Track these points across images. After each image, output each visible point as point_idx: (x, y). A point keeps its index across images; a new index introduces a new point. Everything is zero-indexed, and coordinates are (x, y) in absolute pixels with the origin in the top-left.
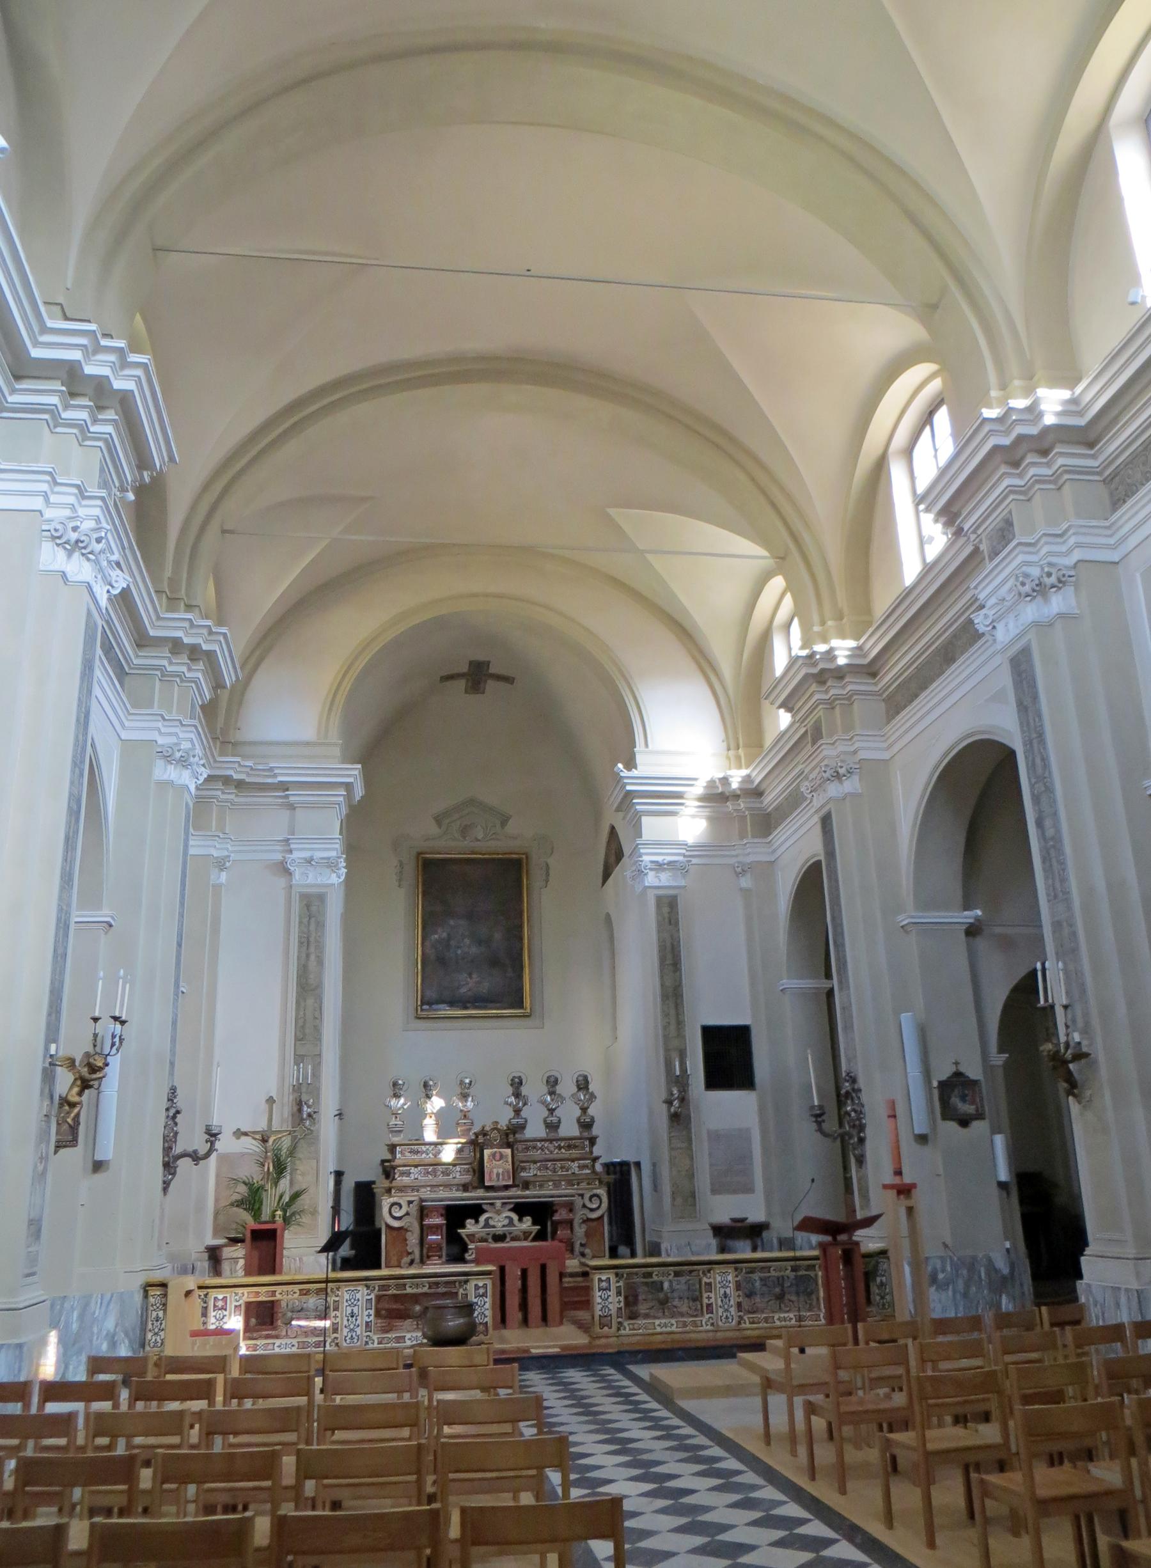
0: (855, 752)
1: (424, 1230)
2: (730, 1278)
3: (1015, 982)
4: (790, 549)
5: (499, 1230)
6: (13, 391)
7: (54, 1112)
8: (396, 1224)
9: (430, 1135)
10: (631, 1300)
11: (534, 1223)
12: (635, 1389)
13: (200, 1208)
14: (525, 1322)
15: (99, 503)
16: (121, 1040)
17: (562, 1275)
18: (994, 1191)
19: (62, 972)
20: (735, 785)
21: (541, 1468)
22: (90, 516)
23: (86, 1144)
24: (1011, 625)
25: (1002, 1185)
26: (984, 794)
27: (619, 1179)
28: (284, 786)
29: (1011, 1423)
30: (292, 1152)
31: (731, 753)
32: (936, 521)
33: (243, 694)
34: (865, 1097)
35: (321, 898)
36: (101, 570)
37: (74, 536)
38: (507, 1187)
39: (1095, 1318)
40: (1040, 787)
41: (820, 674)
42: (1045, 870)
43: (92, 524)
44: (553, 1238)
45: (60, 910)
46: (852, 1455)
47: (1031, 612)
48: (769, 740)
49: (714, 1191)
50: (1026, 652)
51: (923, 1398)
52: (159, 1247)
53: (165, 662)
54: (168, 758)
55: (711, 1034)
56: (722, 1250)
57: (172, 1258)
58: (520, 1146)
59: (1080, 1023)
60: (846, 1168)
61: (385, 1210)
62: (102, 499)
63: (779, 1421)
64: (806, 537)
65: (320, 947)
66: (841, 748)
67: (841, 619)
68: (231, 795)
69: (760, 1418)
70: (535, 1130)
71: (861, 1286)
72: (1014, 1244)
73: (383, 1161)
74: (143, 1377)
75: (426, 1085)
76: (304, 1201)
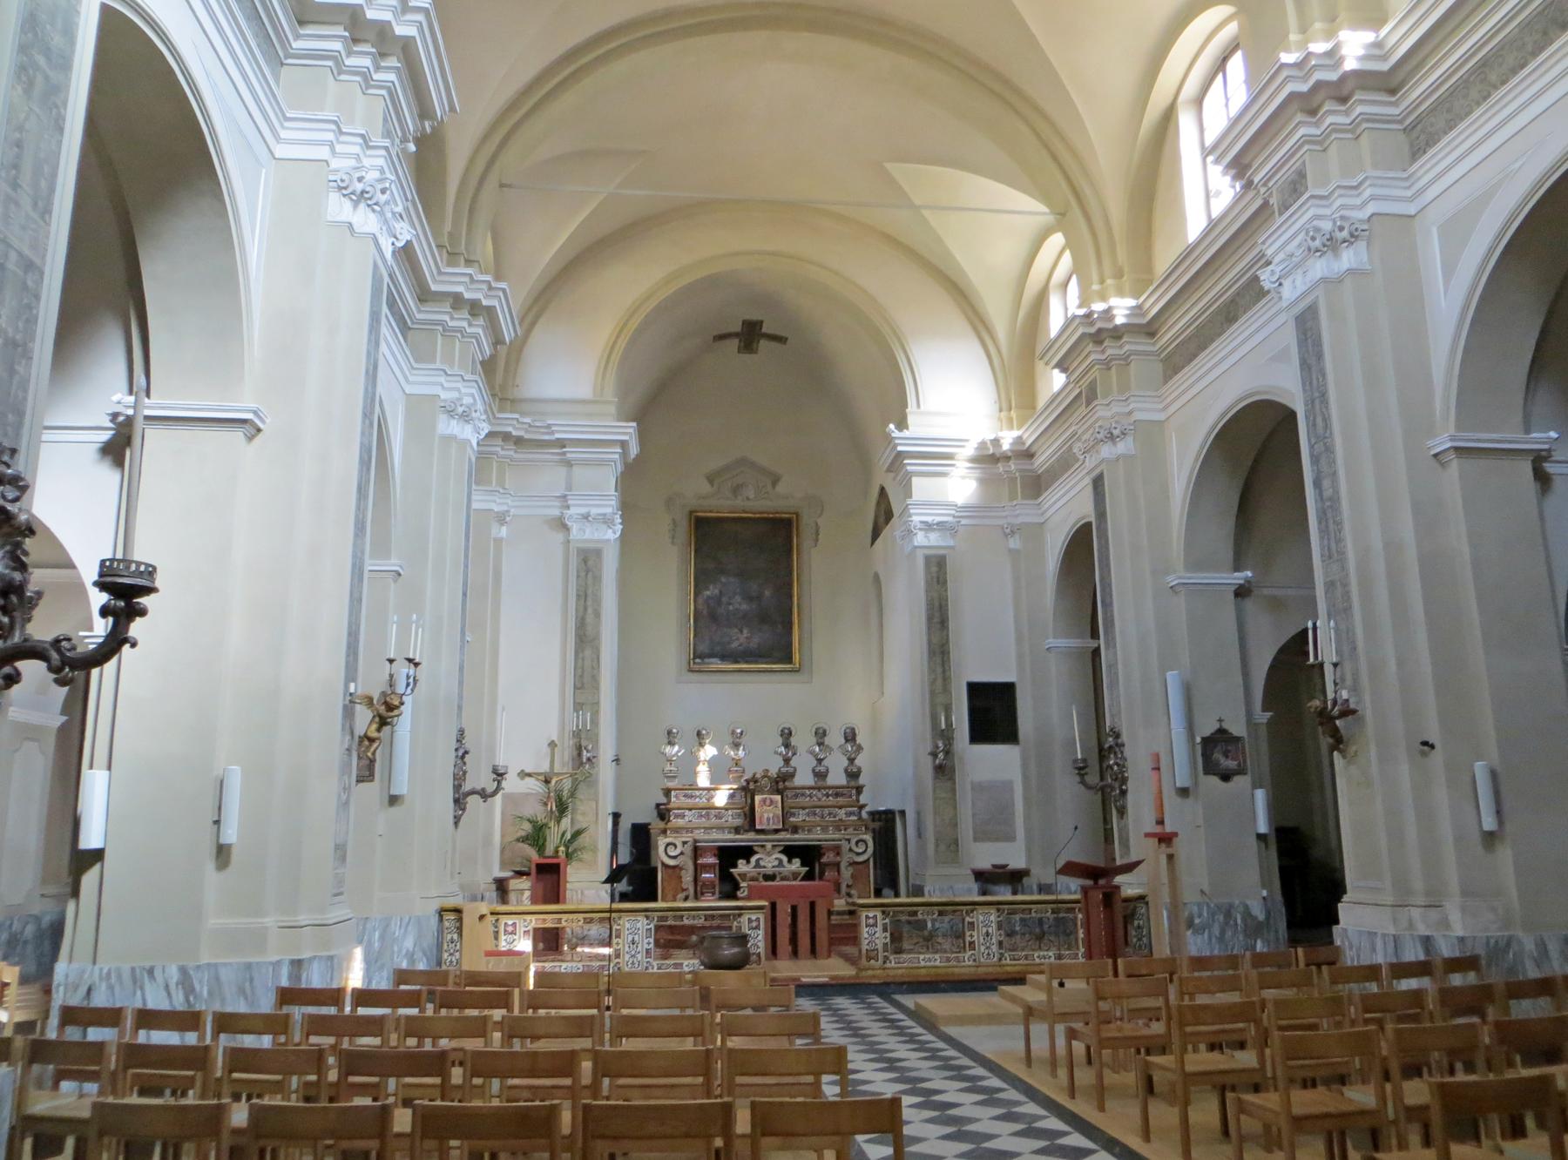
0: (1130, 413)
1: (698, 868)
2: (992, 918)
3: (1283, 640)
4: (1071, 201)
5: (769, 871)
6: (298, 37)
7: (355, 746)
8: (672, 862)
9: (703, 780)
10: (896, 938)
11: (803, 865)
12: (901, 1016)
13: (488, 842)
14: (795, 953)
15: (383, 152)
16: (415, 681)
17: (830, 913)
18: (1253, 841)
19: (358, 618)
20: (1006, 446)
21: (818, 1075)
22: (376, 166)
23: (382, 781)
24: (1298, 282)
25: (1261, 837)
26: (1260, 459)
27: (885, 825)
28: (562, 443)
29: (1268, 1051)
30: (572, 794)
31: (1004, 414)
32: (1225, 173)
33: (521, 350)
34: (1127, 751)
35: (598, 553)
36: (386, 221)
37: (359, 187)
38: (777, 831)
39: (1350, 958)
40: (1319, 447)
41: (1097, 333)
42: (1320, 531)
43: (376, 175)
44: (821, 878)
45: (354, 556)
46: (1110, 1078)
47: (1320, 267)
48: (1042, 402)
49: (976, 840)
50: (1312, 310)
51: (1182, 1025)
52: (452, 876)
53: (446, 318)
54: (451, 413)
55: (977, 691)
56: (984, 893)
57: (462, 887)
58: (789, 793)
59: (1349, 682)
60: (1106, 820)
61: (661, 849)
62: (386, 148)
63: (1040, 1046)
64: (1087, 192)
65: (598, 601)
66: (1116, 408)
67: (1122, 276)
68: (510, 452)
69: (1021, 1045)
70: (804, 778)
71: (1120, 925)
72: (1270, 892)
73: (658, 805)
74: (442, 990)
75: (699, 734)
76: (583, 840)
